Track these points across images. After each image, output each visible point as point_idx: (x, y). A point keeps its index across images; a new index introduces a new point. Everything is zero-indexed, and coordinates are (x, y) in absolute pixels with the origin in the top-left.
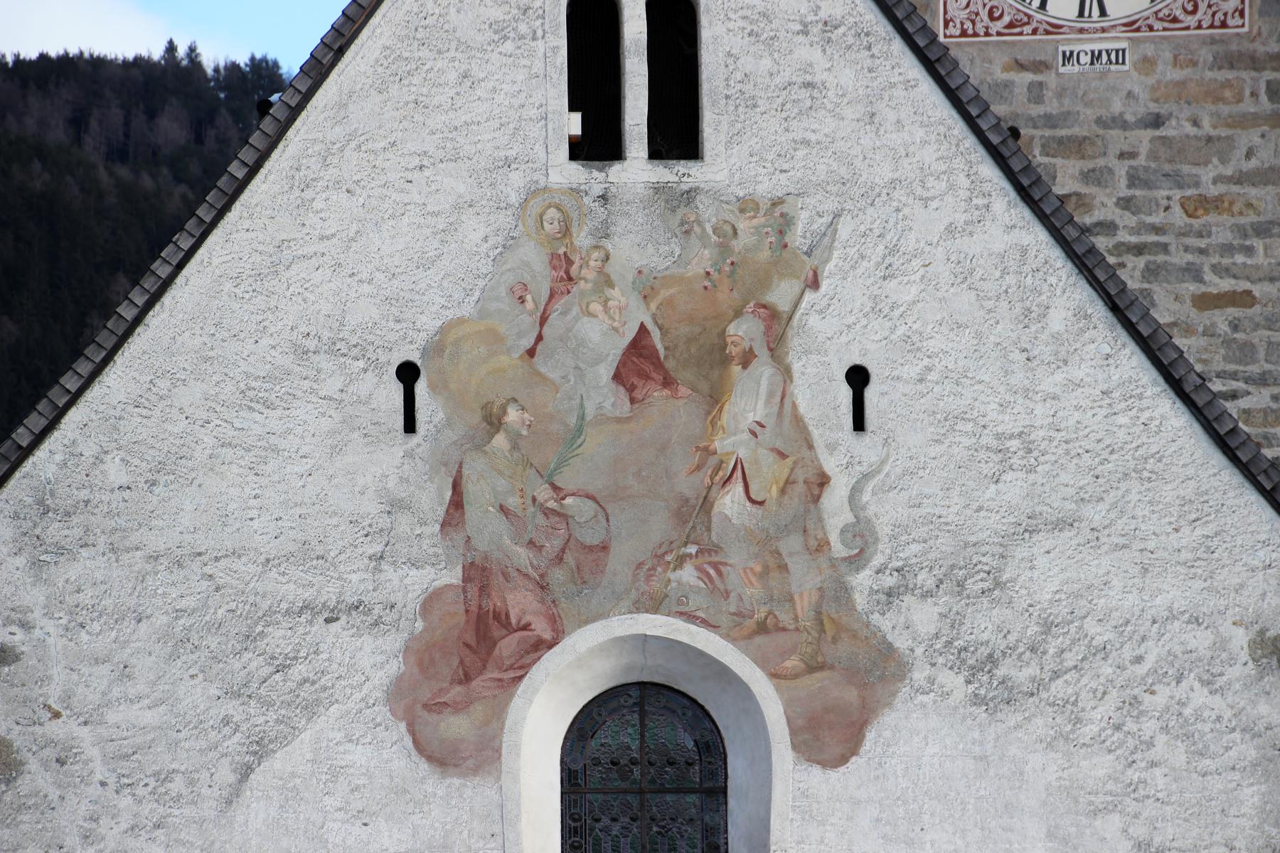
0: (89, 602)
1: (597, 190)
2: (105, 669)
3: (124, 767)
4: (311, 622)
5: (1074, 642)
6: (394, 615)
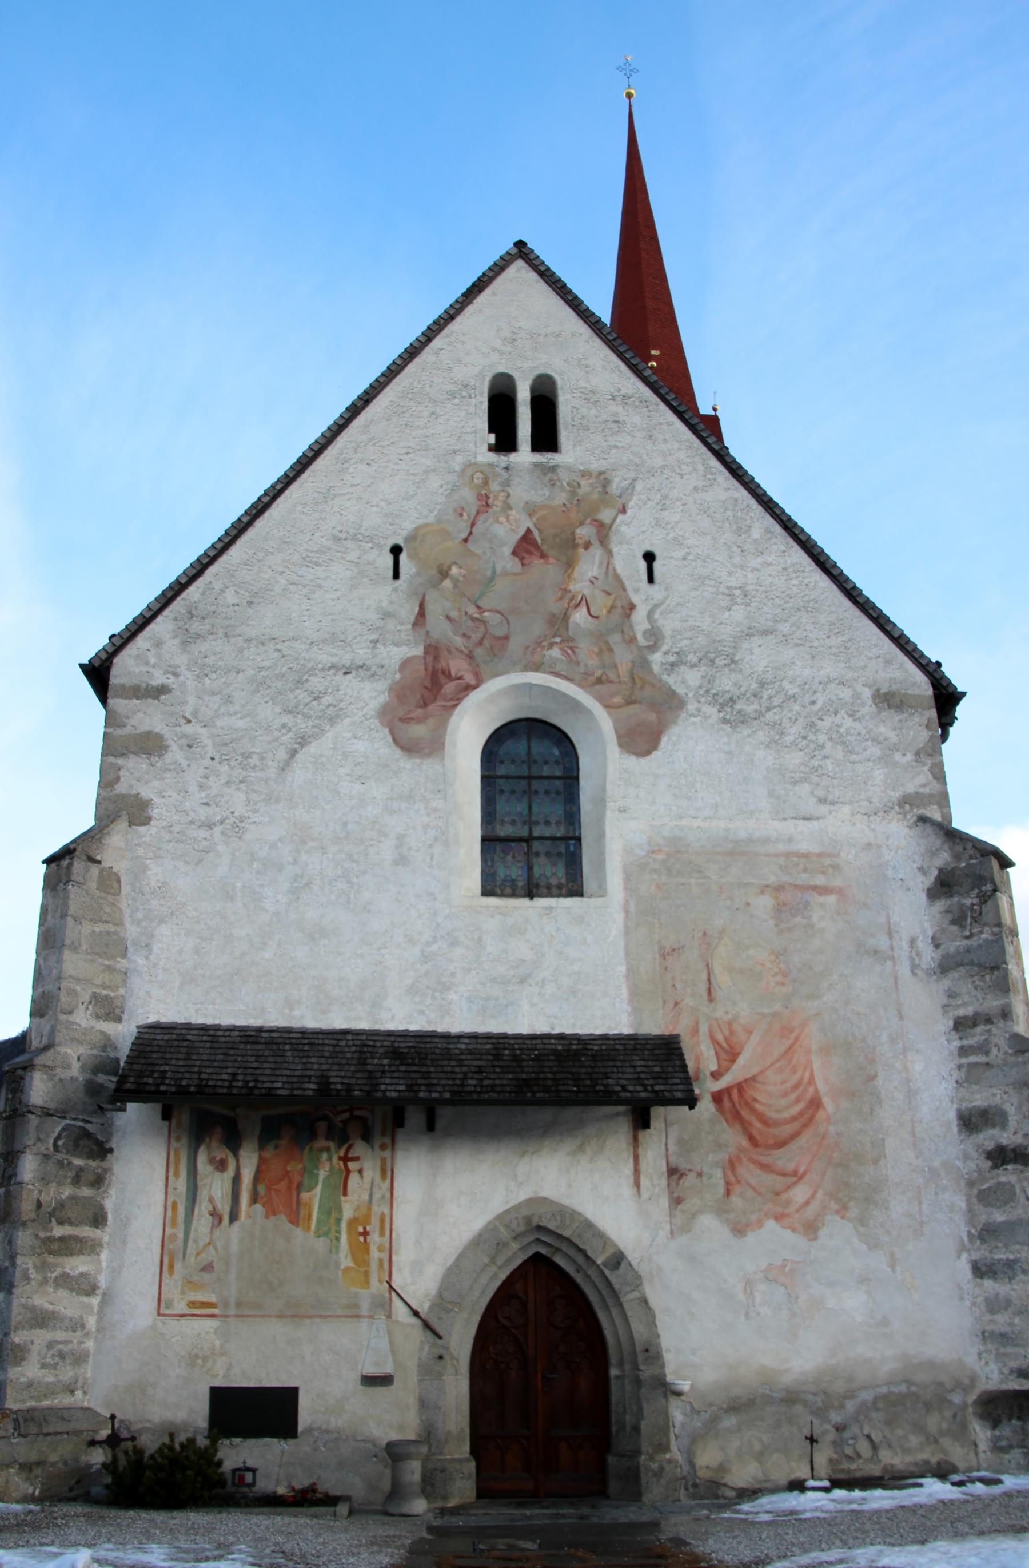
0: (211, 663)
1: (504, 465)
2: (217, 698)
3: (225, 750)
4: (335, 675)
5: (777, 692)
6: (383, 671)
